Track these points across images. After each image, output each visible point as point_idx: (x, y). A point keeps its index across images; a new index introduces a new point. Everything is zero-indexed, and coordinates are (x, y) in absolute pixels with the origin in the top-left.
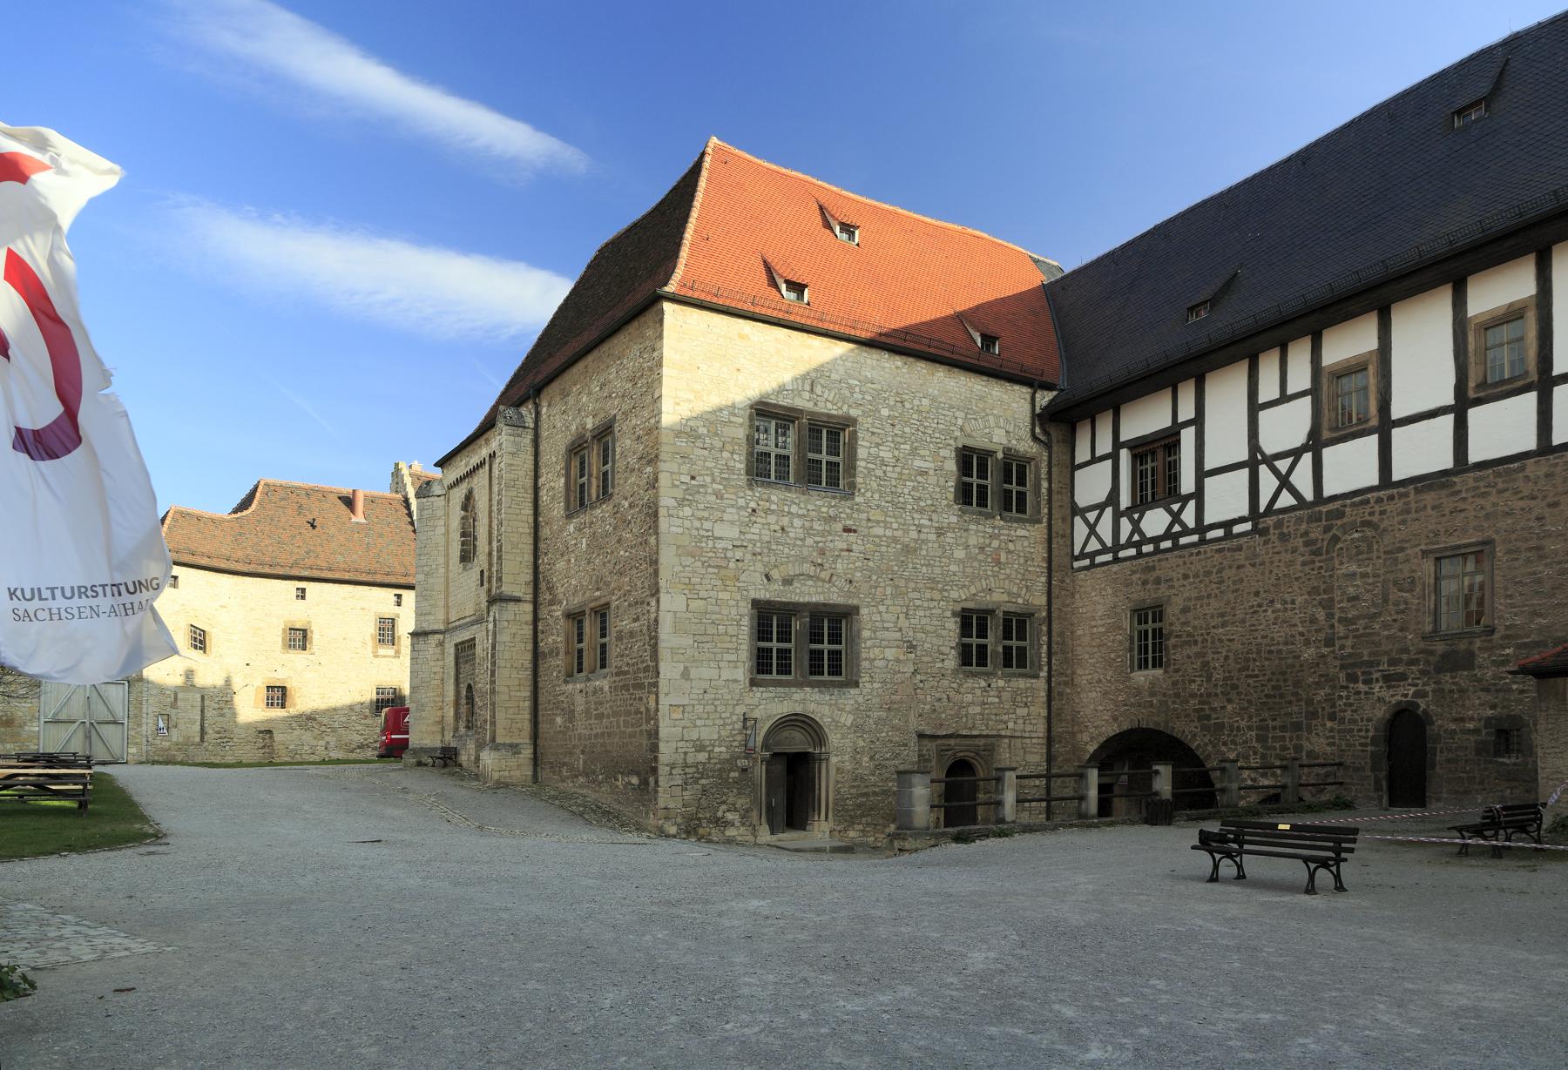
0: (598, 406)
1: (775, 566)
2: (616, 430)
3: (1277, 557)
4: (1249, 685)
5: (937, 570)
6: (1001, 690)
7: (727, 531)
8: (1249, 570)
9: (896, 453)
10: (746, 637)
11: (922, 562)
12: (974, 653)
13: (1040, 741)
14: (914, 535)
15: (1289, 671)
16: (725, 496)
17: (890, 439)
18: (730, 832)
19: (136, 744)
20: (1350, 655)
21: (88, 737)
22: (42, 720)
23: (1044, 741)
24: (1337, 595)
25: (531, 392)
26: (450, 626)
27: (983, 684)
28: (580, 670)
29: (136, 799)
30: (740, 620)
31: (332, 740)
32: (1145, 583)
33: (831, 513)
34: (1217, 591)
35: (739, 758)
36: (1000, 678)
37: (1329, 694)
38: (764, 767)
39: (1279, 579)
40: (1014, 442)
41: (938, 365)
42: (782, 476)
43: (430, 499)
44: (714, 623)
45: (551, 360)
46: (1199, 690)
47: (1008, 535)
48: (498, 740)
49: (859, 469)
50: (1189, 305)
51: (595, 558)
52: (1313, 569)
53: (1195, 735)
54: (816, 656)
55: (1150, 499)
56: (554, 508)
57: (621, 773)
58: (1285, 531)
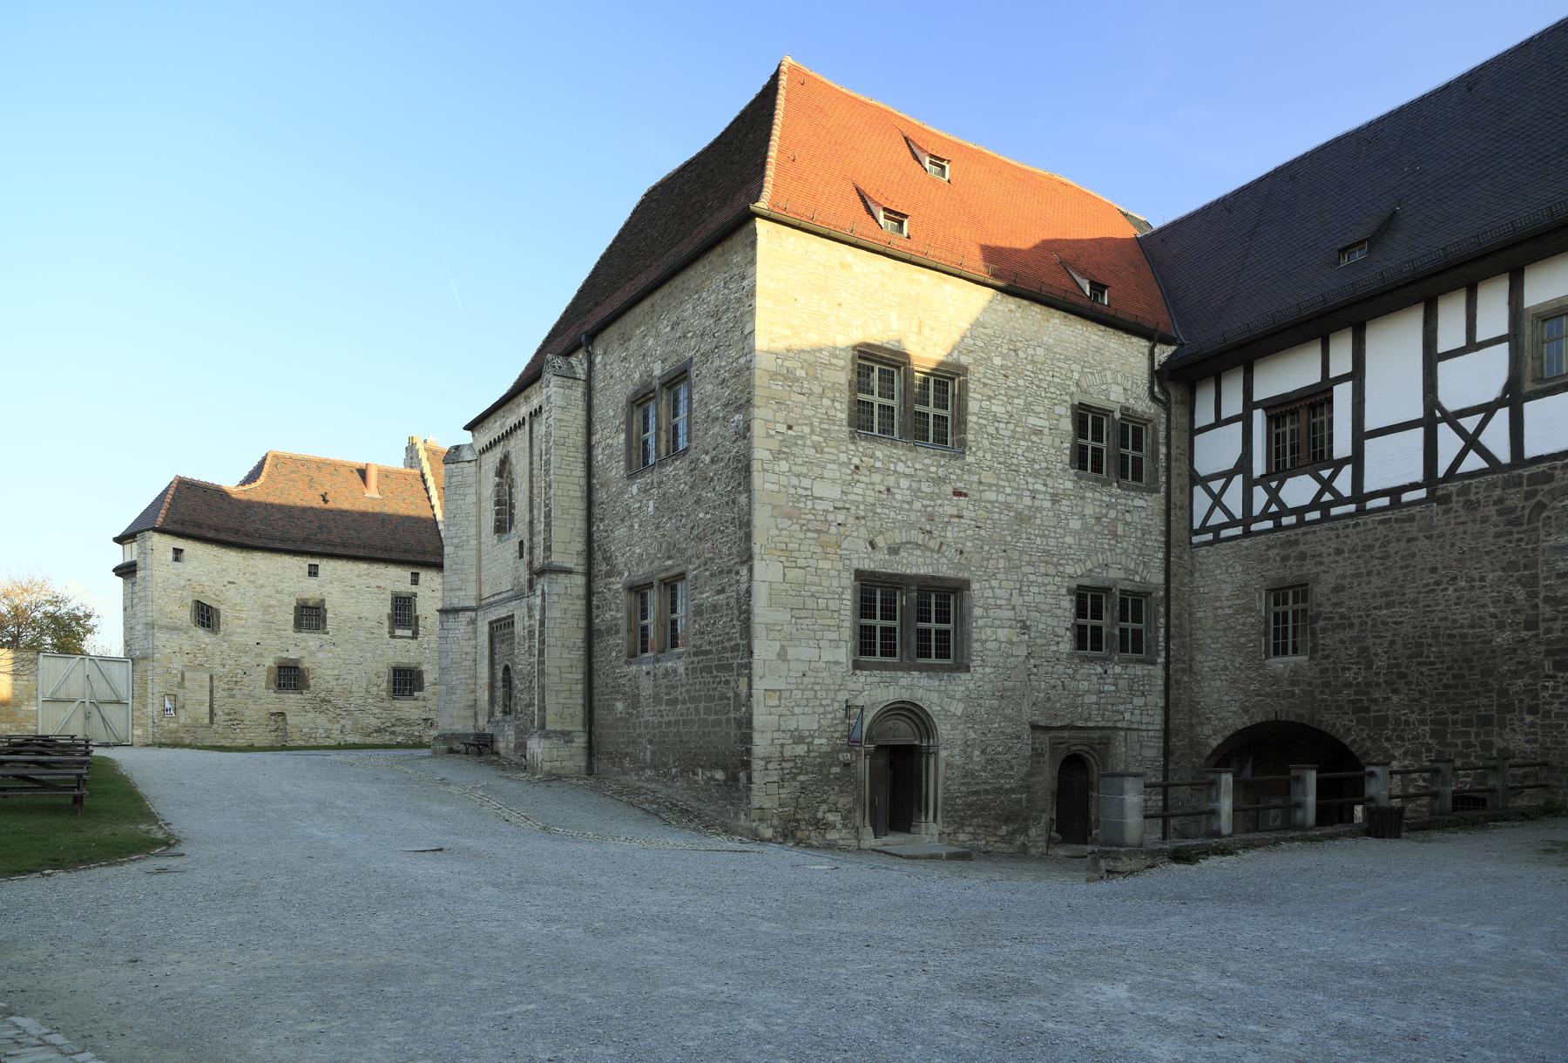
0: (669, 348)
1: (881, 532)
2: (693, 375)
3: (1461, 528)
4: (1422, 674)
5: (1052, 542)
6: (1117, 677)
7: (829, 491)
8: (1423, 544)
9: (1009, 408)
10: (849, 613)
11: (1037, 532)
12: (1089, 636)
13: (1158, 734)
14: (1027, 501)
15: (1476, 657)
16: (826, 450)
17: (1003, 392)
18: (832, 836)
19: (142, 725)
20: (1559, 640)
21: (87, 717)
22: (41, 699)
23: (1161, 734)
24: (1542, 570)
25: (583, 338)
26: (483, 602)
27: (1099, 670)
28: (644, 650)
29: (142, 790)
30: (842, 593)
31: (348, 724)
32: (1285, 559)
33: (940, 474)
34: (1380, 568)
35: (841, 751)
36: (1116, 664)
37: (1530, 684)
38: (868, 761)
39: (1463, 553)
40: (1132, 401)
41: (1053, 310)
42: (886, 430)
43: (460, 465)
44: (814, 596)
45: (597, 309)
46: (1354, 679)
47: (1125, 505)
48: (549, 727)
49: (970, 425)
50: (1340, 246)
51: (666, 523)
52: (1510, 542)
53: (1349, 729)
54: (924, 635)
55: (1288, 466)
56: (613, 468)
57: (702, 767)
58: (1473, 498)
